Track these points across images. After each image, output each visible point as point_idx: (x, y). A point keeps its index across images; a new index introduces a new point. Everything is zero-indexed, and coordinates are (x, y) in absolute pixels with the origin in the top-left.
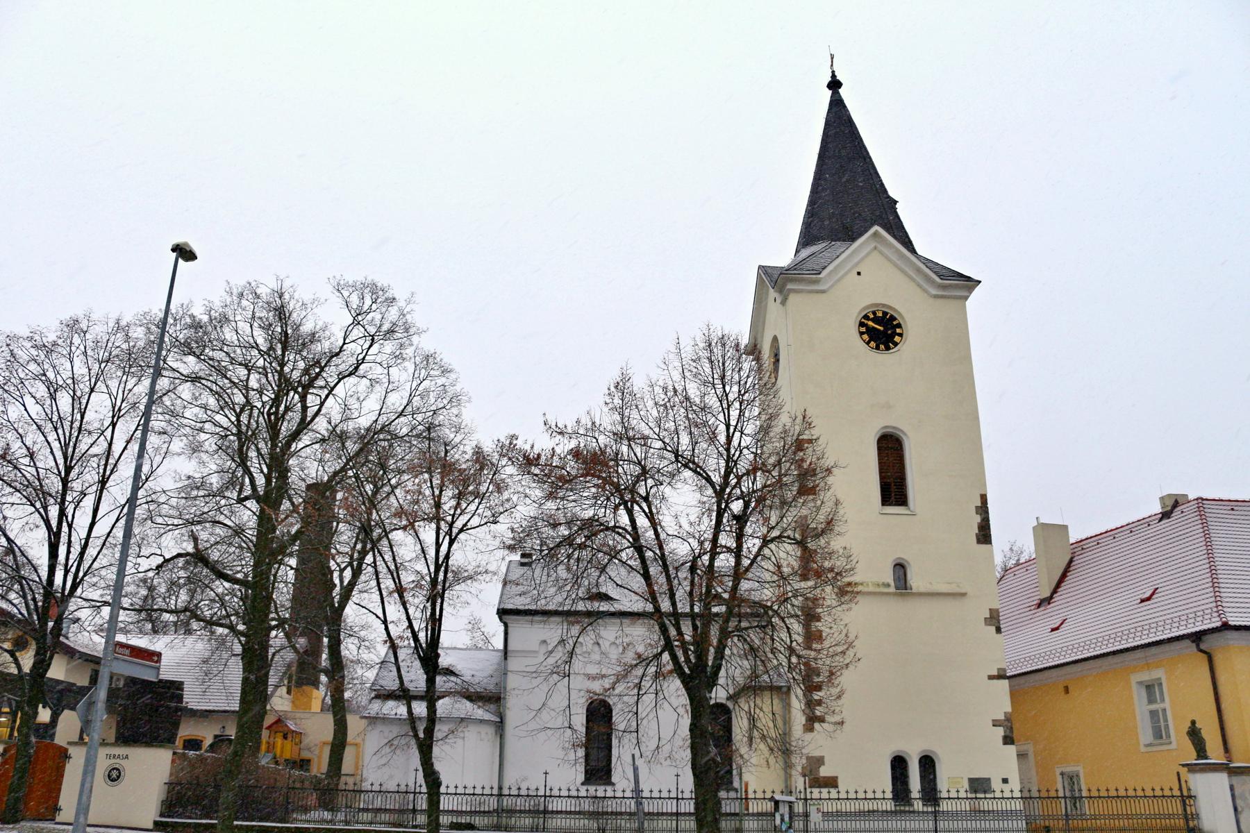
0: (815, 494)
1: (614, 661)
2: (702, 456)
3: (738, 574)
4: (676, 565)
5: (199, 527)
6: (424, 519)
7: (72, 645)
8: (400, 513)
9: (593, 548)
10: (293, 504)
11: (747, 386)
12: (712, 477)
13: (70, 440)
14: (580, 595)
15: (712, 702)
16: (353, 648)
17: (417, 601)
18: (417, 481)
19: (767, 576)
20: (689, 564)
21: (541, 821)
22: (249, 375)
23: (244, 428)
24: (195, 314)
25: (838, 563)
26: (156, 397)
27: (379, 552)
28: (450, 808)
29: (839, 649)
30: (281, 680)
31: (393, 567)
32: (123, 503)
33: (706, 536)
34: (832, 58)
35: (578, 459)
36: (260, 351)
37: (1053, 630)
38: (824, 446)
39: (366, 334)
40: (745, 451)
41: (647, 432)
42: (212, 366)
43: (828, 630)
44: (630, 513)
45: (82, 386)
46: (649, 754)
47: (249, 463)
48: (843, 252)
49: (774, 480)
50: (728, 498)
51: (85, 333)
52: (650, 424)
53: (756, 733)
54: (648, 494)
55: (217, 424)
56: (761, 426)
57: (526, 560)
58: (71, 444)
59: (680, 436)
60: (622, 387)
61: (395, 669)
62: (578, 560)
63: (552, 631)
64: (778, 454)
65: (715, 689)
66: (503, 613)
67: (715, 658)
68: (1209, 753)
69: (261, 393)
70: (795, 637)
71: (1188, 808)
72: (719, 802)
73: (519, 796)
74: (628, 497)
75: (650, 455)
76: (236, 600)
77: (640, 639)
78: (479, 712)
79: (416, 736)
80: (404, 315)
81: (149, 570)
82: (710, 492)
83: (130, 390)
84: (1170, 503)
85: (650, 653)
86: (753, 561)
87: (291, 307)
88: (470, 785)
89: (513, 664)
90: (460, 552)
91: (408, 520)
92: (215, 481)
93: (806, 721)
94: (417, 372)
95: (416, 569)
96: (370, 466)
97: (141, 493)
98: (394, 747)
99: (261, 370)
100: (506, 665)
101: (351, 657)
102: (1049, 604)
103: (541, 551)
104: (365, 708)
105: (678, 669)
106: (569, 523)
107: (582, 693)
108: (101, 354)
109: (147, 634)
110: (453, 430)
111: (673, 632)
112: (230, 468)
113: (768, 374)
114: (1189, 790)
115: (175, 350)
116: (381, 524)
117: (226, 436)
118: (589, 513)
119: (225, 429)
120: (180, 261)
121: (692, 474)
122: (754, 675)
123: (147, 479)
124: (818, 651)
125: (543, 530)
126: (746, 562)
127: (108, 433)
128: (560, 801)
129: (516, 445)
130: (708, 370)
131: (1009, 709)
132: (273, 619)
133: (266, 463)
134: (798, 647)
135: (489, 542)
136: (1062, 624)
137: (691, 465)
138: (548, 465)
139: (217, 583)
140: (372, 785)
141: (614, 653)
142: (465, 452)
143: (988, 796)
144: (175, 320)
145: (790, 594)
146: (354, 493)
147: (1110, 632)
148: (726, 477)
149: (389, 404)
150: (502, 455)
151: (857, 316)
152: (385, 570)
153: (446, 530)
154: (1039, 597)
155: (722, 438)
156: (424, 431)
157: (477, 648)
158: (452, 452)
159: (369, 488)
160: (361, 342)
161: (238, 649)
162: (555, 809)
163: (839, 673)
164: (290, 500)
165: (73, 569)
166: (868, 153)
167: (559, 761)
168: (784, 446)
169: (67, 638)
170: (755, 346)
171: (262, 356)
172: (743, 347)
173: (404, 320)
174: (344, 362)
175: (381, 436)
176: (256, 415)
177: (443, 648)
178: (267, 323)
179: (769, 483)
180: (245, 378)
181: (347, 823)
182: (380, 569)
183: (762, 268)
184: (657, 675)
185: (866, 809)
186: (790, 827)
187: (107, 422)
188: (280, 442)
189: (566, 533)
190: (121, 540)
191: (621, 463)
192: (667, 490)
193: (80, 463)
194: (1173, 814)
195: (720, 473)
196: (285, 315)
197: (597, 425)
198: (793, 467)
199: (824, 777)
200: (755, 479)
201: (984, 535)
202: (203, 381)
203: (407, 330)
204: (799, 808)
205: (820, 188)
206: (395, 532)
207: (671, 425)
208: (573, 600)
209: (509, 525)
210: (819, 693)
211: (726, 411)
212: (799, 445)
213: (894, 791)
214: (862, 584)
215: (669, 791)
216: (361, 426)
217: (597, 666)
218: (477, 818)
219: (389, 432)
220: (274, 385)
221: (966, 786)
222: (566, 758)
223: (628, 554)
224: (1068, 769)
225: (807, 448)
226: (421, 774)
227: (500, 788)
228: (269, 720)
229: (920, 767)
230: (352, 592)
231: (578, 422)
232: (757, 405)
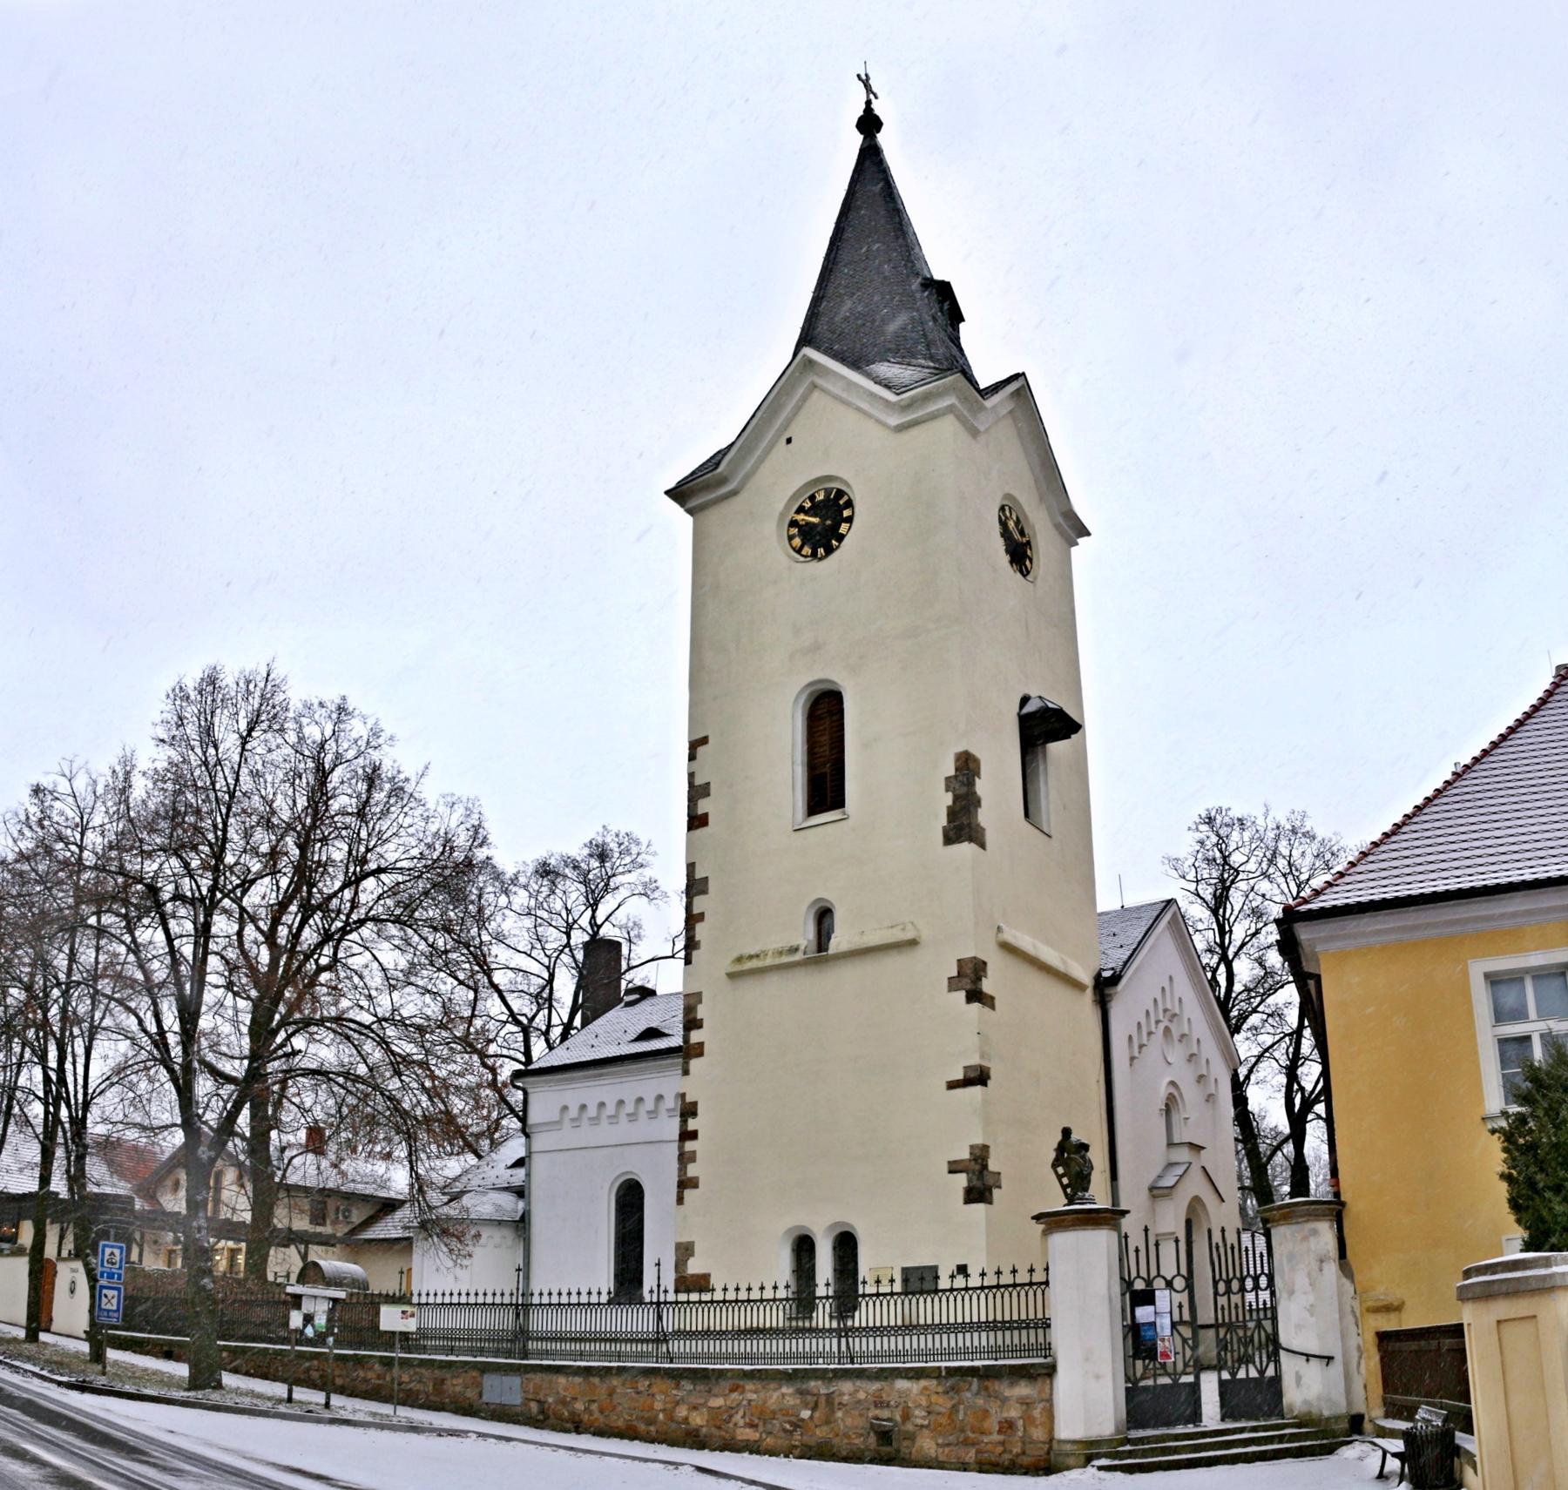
199: (693, 1276)
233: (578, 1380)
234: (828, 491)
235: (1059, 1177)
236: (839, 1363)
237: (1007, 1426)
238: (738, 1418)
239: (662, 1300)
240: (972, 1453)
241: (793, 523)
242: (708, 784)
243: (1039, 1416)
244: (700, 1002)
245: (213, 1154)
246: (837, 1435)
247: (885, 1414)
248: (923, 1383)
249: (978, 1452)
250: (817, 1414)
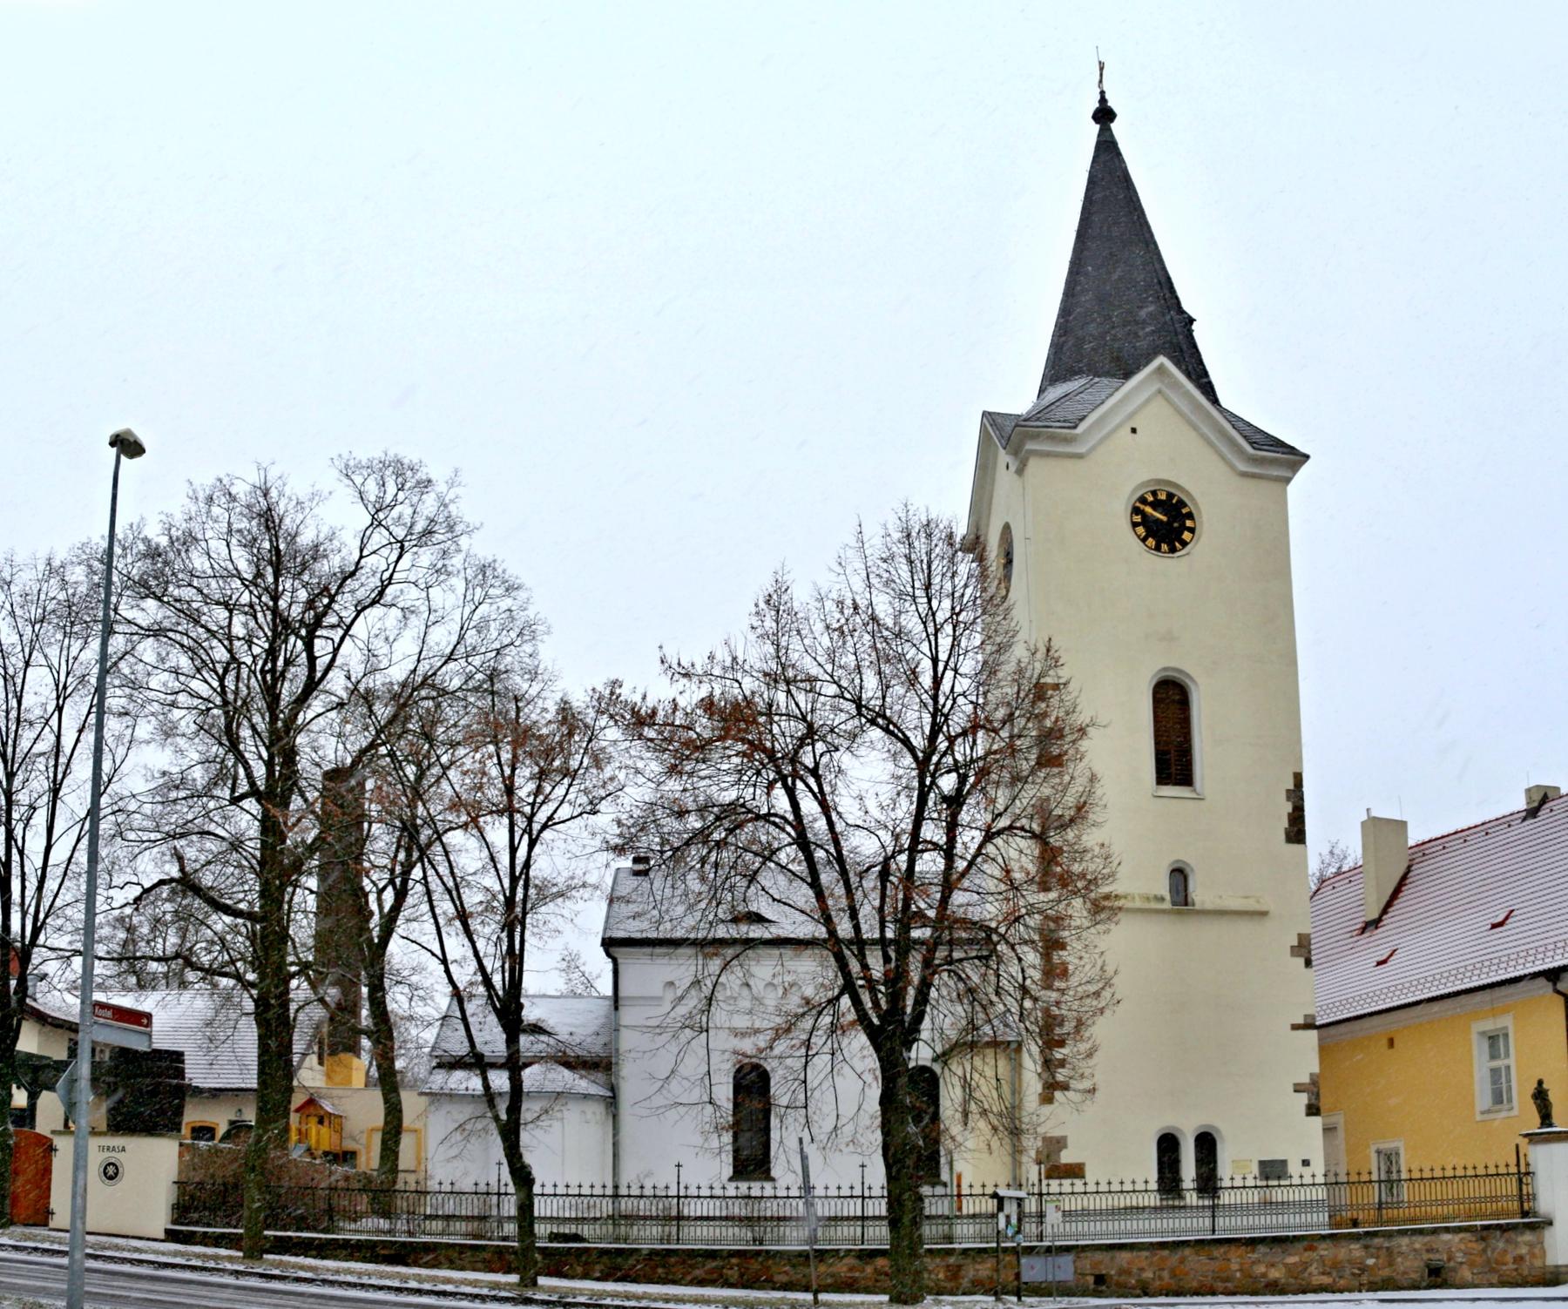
0: (1061, 765)
1: (771, 1009)
2: (897, 708)
3: (949, 883)
4: (859, 869)
5: (183, 842)
6: (491, 812)
7: (41, 1008)
8: (457, 804)
9: (737, 847)
10: (306, 800)
11: (965, 601)
12: (912, 739)
13: (7, 737)
14: (721, 915)
15: (912, 1064)
16: (403, 1000)
17: (487, 930)
18: (478, 756)
19: (991, 885)
20: (878, 868)
21: (674, 1230)
22: (231, 618)
23: (231, 697)
24: (149, 537)
25: (1092, 867)
26: (109, 664)
27: (430, 862)
28: (549, 1215)
29: (1092, 988)
30: (309, 1046)
31: (451, 884)
32: (83, 816)
33: (903, 826)
34: (1102, 69)
35: (712, 714)
36: (242, 580)
37: (1379, 963)
38: (1075, 694)
39: (393, 540)
40: (961, 700)
41: (815, 671)
42: (179, 610)
43: (1076, 961)
44: (791, 793)
45: (13, 660)
46: (824, 1137)
47: (242, 747)
48: (1111, 395)
49: (1003, 744)
50: (936, 770)
51: (9, 584)
52: (818, 658)
53: (973, 1107)
54: (817, 764)
55: (194, 695)
56: (985, 663)
57: (641, 867)
58: (10, 742)
59: (864, 677)
60: (776, 603)
61: (461, 1027)
62: (716, 865)
63: (682, 968)
64: (1009, 704)
65: (915, 1046)
66: (610, 945)
67: (916, 1002)
68: (1555, 1120)
69: (250, 643)
70: (1030, 972)
71: (1524, 1187)
72: (920, 1199)
73: (642, 1197)
74: (787, 769)
75: (819, 706)
76: (241, 939)
77: (809, 977)
78: (581, 1083)
79: (496, 1118)
80: (446, 506)
81: (125, 905)
82: (908, 760)
83: (75, 659)
84: (1537, 797)
85: (823, 996)
86: (971, 864)
87: (281, 509)
88: (574, 1183)
89: (628, 1016)
90: (544, 857)
91: (469, 814)
92: (199, 776)
93: (1044, 1088)
94: (470, 592)
95: (480, 889)
96: (410, 737)
97: (104, 800)
98: (466, 1133)
99: (246, 609)
100: (617, 1019)
101: (400, 1012)
102: (1377, 928)
103: (662, 852)
104: (425, 1082)
105: (863, 1018)
106: (702, 810)
107: (727, 1056)
108: (33, 612)
109: (131, 990)
110: (527, 676)
111: (855, 967)
112: (216, 756)
113: (996, 582)
114: (1528, 1165)
115: (128, 593)
116: (430, 821)
117: (209, 709)
118: (729, 796)
119: (205, 699)
120: (123, 458)
121: (883, 734)
122: (972, 1026)
123: (110, 781)
124: (1062, 992)
125: (663, 822)
126: (961, 865)
127: (54, 722)
128: (699, 1203)
129: (620, 695)
130: (906, 575)
131: (1316, 1070)
132: (292, 964)
133: (264, 744)
134: (1034, 986)
135: (586, 842)
136: (1391, 955)
137: (880, 721)
138: (669, 725)
139: (214, 917)
140: (440, 1184)
141: (771, 999)
142: (545, 710)
143: (1282, 1183)
144: (124, 549)
145: (1023, 911)
146: (390, 779)
147: (1537, 944)
148: (935, 730)
149: (432, 644)
150: (600, 712)
151: (1129, 499)
152: (441, 889)
153: (523, 826)
154: (1363, 919)
155: (926, 680)
156: (484, 682)
157: (575, 995)
158: (526, 710)
159: (411, 771)
160: (385, 552)
161: (249, 1005)
162: (692, 1214)
163: (1090, 1022)
164: (302, 795)
165: (32, 910)
166: (1152, 235)
167: (697, 1150)
168: (1018, 693)
169: (35, 1000)
170: (978, 538)
171: (247, 587)
172: (958, 540)
173: (446, 514)
174: (362, 585)
175: (423, 693)
176: (245, 676)
177: (527, 996)
178: (249, 537)
179: (995, 747)
180: (225, 623)
181: (410, 1234)
182: (433, 886)
183: (986, 415)
184: (833, 1029)
185: (1122, 1205)
186: (1018, 1232)
187: (51, 707)
188: (282, 711)
189: (698, 825)
190: (85, 866)
191: (776, 718)
192: (844, 758)
193: (24, 767)
194: (1502, 1196)
195: (923, 733)
196: (273, 522)
197: (740, 661)
198: (1030, 725)
199: (1066, 1165)
200: (974, 742)
201: (1296, 832)
202: (171, 634)
203: (451, 528)
204: (1031, 1206)
205: (1079, 288)
206: (450, 834)
207: (850, 660)
208: (711, 923)
209: (614, 816)
210: (1062, 1050)
211: (932, 638)
212: (1040, 692)
213: (1161, 1180)
214: (1125, 897)
215: (852, 1188)
216: (394, 681)
217: (747, 1017)
218: (586, 1227)
219: (433, 686)
220: (266, 630)
221: (1255, 1170)
222: (706, 1146)
223: (786, 855)
224: (1387, 1146)
225: (1052, 697)
226: (505, 1169)
227: (616, 1187)
228: (298, 1100)
229: (1196, 1146)
230: (395, 921)
231: (711, 657)
232: (979, 629)
233: (1145, 1254)
237: (1519, 1259)
238: (1313, 1269)
248: (1462, 1235)
250: (1381, 1261)
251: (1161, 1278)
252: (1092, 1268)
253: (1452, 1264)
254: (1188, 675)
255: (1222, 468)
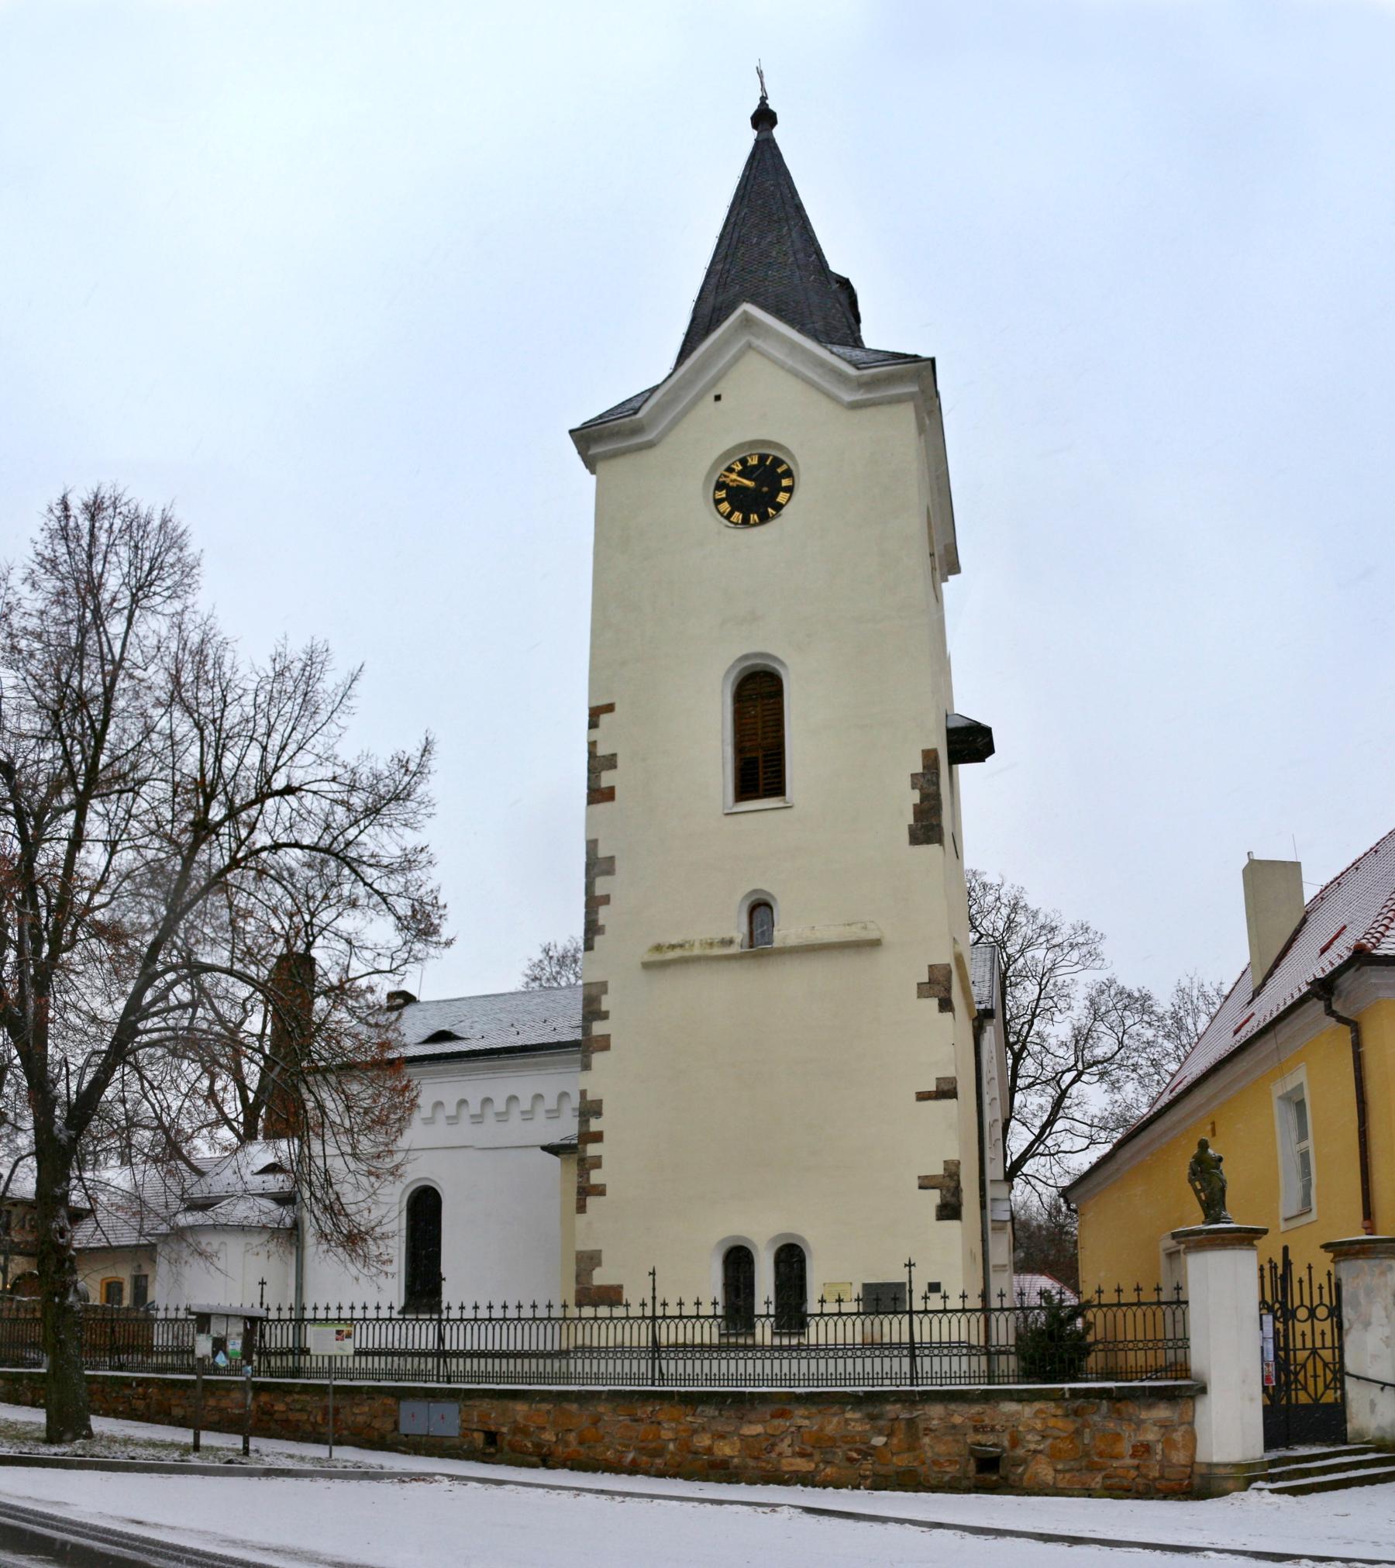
199: (600, 1287)
233: (546, 1407)
234: (763, 458)
235: (1197, 1192)
236: (912, 1385)
238: (784, 1446)
239: (659, 1312)
240: (1099, 1478)
241: (720, 486)
242: (614, 755)
243: (1180, 1439)
244: (605, 992)
245: (72, 1133)
246: (924, 1463)
247: (991, 1439)
248: (1038, 1405)
249: (1106, 1477)
250: (895, 1441)
251: (567, 1444)
252: (479, 1421)
253: (1020, 1452)
254: (775, 659)
255: (826, 405)
